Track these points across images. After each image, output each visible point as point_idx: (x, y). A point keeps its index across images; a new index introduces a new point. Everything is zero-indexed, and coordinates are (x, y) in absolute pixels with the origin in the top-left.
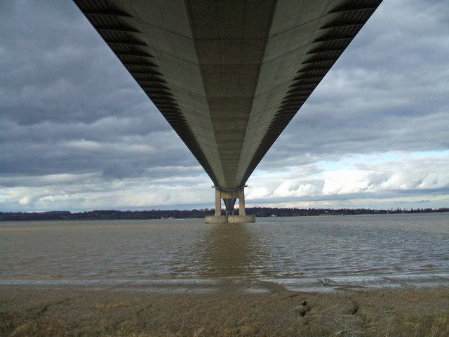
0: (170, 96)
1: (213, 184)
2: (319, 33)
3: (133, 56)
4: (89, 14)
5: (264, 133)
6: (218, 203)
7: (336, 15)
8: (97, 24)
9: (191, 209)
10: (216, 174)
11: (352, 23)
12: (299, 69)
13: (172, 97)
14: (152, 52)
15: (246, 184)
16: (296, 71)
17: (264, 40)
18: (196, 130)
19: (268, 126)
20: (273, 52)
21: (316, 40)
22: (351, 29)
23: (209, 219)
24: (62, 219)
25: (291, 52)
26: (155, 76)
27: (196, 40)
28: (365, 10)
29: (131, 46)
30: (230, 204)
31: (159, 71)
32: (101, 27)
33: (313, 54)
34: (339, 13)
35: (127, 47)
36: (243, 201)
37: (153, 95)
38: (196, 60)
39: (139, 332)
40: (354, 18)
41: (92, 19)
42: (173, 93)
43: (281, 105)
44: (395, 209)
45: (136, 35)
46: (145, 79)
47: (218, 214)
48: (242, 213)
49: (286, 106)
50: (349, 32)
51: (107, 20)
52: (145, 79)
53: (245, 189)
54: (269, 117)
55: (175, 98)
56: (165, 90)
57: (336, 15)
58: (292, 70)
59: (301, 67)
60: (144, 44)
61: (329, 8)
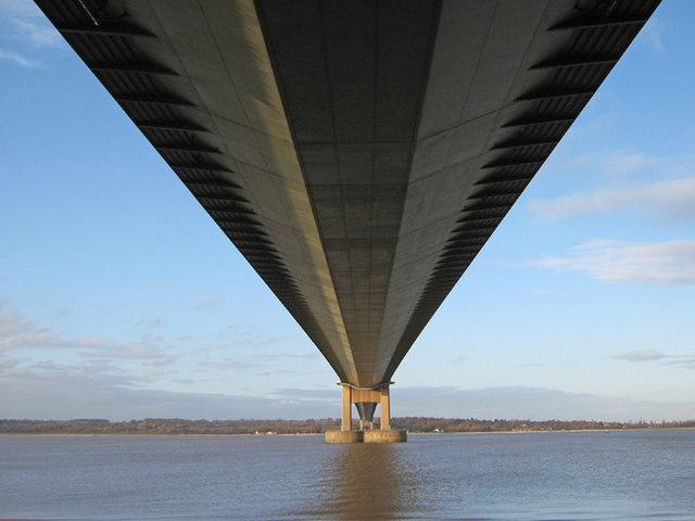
0: (264, 237)
2: (502, 134)
3: (187, 152)
4: (102, 70)
5: (418, 298)
9: (304, 418)
11: (527, 161)
12: (532, 64)
13: (263, 229)
14: (229, 164)
15: (392, 380)
16: (450, 230)
17: (411, 142)
19: (423, 287)
21: (497, 146)
22: (553, 127)
23: (331, 436)
25: (457, 164)
26: (238, 202)
28: (574, 96)
30: (368, 409)
31: (240, 194)
32: (164, 145)
33: (491, 170)
34: (551, 69)
35: (189, 155)
41: (168, 156)
42: (267, 232)
43: (440, 259)
44: (635, 421)
45: (202, 135)
46: (222, 208)
47: (345, 426)
48: (384, 425)
49: (462, 237)
50: (551, 133)
51: (142, 82)
52: (222, 208)
54: (425, 272)
55: (271, 239)
56: (257, 227)
59: (473, 189)
60: (216, 151)
61: (517, 93)
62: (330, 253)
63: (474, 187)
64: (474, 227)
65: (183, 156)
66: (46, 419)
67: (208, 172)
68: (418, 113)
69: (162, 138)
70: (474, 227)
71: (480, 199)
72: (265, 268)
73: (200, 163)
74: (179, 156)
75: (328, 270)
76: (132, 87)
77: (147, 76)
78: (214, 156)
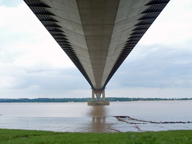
1: (91, 87)
2: (137, 22)
3: (53, 27)
6: (93, 96)
7: (136, 27)
8: (40, 19)
10: (78, 52)
11: (138, 37)
13: (74, 52)
15: (106, 87)
17: (113, 25)
18: (64, 25)
20: (108, 58)
21: (135, 25)
24: (25, 102)
27: (83, 25)
29: (55, 28)
33: (126, 45)
34: (145, 14)
36: (104, 95)
37: (65, 48)
38: (83, 33)
39: (70, 143)
40: (151, 16)
43: (121, 53)
53: (105, 89)
57: (136, 27)
58: (125, 38)
59: (129, 37)
60: (61, 27)
61: (141, 12)
62: (87, 41)
63: (136, 21)
64: (125, 53)
65: (50, 23)
66: (12, 98)
67: (61, 37)
68: (115, 17)
69: (39, 11)
70: (125, 53)
71: (131, 39)
72: (70, 56)
73: (56, 30)
74: (51, 28)
75: (87, 46)
76: (39, 11)
77: (44, 8)
78: (60, 28)
